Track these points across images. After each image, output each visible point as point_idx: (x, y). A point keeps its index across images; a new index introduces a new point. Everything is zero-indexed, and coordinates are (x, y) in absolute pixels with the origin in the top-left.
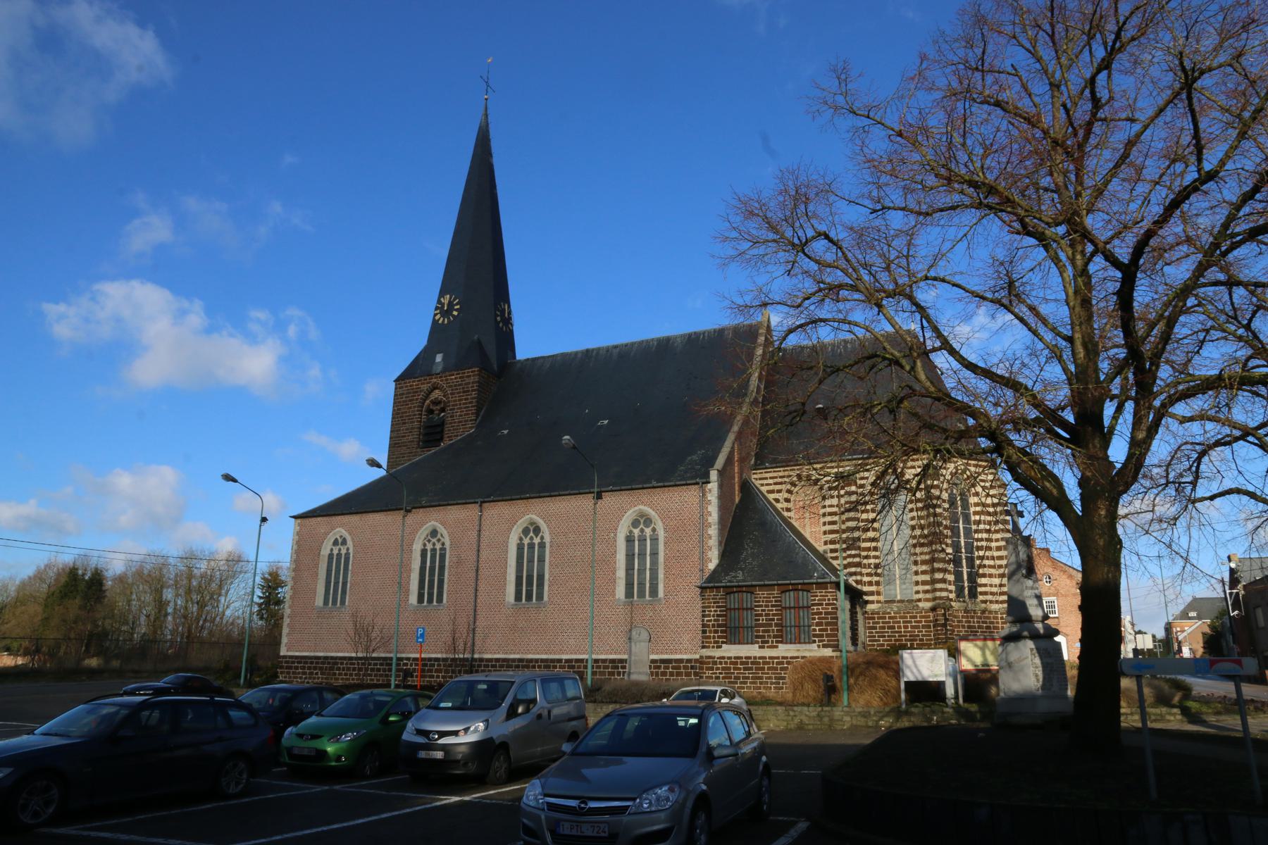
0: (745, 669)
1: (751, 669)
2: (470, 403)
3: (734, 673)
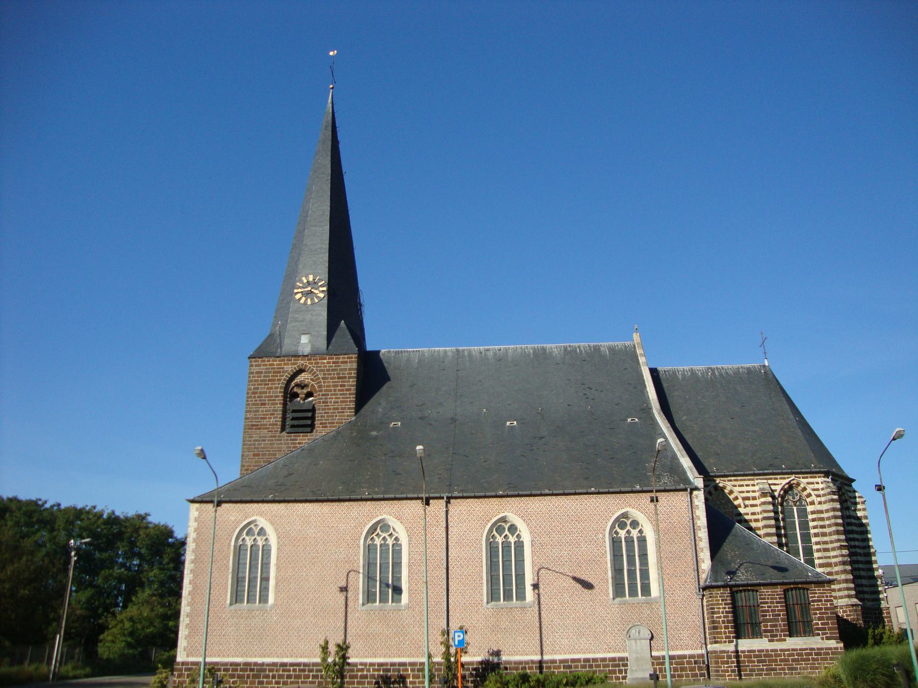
0: (759, 662)
1: (764, 661)
2: (347, 390)
3: (749, 666)
